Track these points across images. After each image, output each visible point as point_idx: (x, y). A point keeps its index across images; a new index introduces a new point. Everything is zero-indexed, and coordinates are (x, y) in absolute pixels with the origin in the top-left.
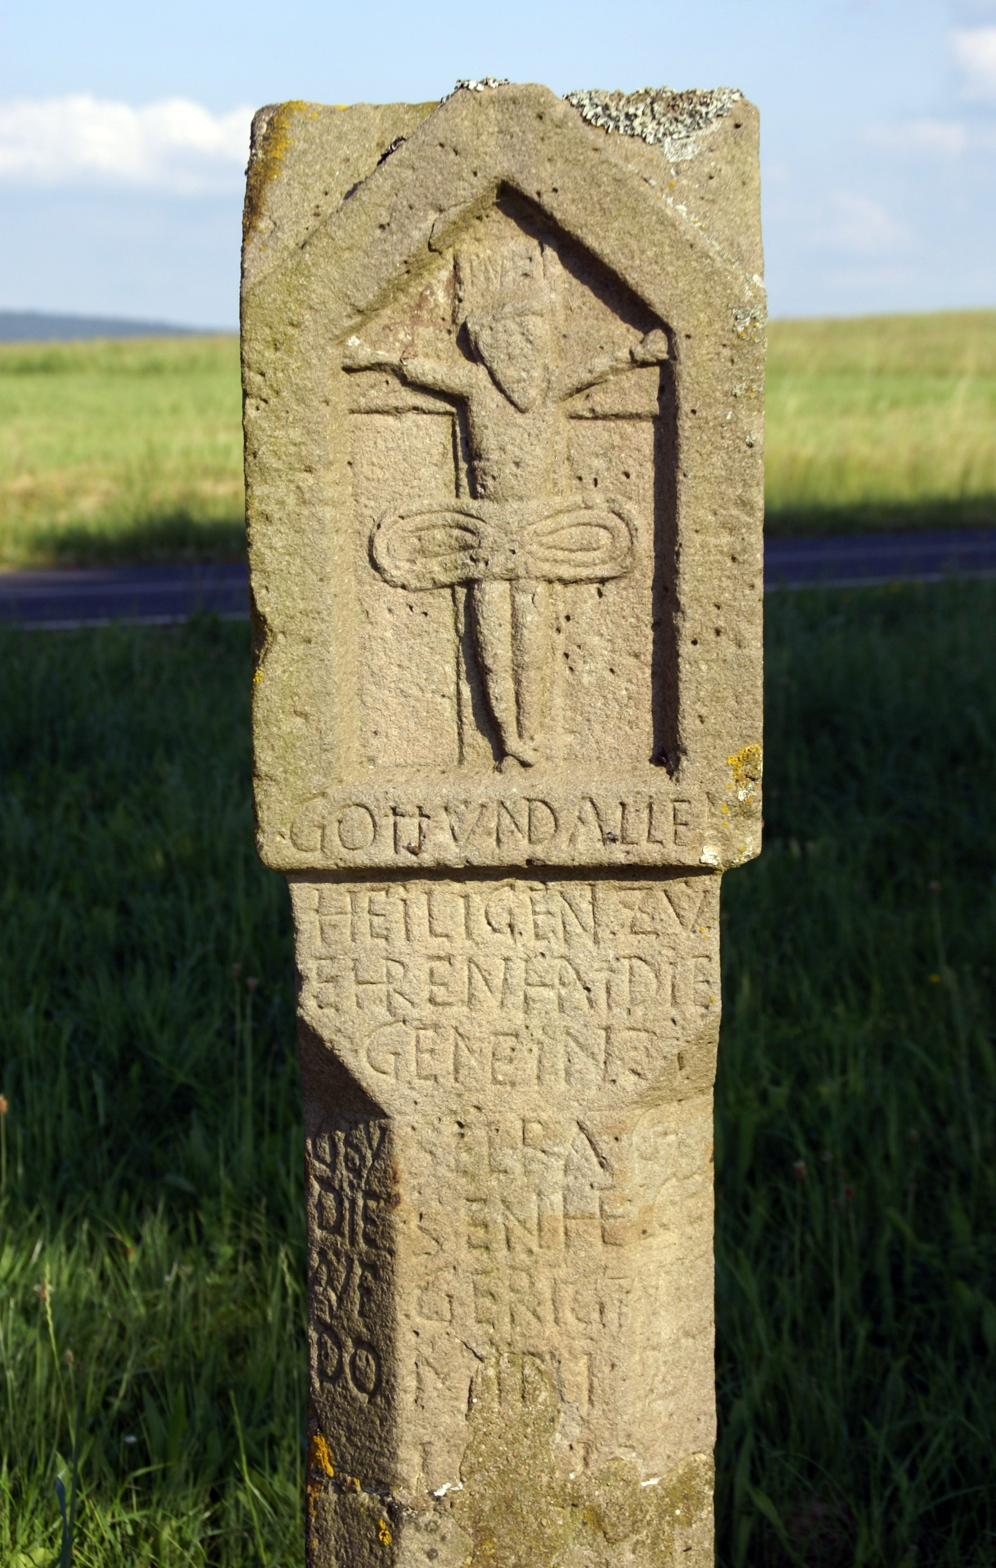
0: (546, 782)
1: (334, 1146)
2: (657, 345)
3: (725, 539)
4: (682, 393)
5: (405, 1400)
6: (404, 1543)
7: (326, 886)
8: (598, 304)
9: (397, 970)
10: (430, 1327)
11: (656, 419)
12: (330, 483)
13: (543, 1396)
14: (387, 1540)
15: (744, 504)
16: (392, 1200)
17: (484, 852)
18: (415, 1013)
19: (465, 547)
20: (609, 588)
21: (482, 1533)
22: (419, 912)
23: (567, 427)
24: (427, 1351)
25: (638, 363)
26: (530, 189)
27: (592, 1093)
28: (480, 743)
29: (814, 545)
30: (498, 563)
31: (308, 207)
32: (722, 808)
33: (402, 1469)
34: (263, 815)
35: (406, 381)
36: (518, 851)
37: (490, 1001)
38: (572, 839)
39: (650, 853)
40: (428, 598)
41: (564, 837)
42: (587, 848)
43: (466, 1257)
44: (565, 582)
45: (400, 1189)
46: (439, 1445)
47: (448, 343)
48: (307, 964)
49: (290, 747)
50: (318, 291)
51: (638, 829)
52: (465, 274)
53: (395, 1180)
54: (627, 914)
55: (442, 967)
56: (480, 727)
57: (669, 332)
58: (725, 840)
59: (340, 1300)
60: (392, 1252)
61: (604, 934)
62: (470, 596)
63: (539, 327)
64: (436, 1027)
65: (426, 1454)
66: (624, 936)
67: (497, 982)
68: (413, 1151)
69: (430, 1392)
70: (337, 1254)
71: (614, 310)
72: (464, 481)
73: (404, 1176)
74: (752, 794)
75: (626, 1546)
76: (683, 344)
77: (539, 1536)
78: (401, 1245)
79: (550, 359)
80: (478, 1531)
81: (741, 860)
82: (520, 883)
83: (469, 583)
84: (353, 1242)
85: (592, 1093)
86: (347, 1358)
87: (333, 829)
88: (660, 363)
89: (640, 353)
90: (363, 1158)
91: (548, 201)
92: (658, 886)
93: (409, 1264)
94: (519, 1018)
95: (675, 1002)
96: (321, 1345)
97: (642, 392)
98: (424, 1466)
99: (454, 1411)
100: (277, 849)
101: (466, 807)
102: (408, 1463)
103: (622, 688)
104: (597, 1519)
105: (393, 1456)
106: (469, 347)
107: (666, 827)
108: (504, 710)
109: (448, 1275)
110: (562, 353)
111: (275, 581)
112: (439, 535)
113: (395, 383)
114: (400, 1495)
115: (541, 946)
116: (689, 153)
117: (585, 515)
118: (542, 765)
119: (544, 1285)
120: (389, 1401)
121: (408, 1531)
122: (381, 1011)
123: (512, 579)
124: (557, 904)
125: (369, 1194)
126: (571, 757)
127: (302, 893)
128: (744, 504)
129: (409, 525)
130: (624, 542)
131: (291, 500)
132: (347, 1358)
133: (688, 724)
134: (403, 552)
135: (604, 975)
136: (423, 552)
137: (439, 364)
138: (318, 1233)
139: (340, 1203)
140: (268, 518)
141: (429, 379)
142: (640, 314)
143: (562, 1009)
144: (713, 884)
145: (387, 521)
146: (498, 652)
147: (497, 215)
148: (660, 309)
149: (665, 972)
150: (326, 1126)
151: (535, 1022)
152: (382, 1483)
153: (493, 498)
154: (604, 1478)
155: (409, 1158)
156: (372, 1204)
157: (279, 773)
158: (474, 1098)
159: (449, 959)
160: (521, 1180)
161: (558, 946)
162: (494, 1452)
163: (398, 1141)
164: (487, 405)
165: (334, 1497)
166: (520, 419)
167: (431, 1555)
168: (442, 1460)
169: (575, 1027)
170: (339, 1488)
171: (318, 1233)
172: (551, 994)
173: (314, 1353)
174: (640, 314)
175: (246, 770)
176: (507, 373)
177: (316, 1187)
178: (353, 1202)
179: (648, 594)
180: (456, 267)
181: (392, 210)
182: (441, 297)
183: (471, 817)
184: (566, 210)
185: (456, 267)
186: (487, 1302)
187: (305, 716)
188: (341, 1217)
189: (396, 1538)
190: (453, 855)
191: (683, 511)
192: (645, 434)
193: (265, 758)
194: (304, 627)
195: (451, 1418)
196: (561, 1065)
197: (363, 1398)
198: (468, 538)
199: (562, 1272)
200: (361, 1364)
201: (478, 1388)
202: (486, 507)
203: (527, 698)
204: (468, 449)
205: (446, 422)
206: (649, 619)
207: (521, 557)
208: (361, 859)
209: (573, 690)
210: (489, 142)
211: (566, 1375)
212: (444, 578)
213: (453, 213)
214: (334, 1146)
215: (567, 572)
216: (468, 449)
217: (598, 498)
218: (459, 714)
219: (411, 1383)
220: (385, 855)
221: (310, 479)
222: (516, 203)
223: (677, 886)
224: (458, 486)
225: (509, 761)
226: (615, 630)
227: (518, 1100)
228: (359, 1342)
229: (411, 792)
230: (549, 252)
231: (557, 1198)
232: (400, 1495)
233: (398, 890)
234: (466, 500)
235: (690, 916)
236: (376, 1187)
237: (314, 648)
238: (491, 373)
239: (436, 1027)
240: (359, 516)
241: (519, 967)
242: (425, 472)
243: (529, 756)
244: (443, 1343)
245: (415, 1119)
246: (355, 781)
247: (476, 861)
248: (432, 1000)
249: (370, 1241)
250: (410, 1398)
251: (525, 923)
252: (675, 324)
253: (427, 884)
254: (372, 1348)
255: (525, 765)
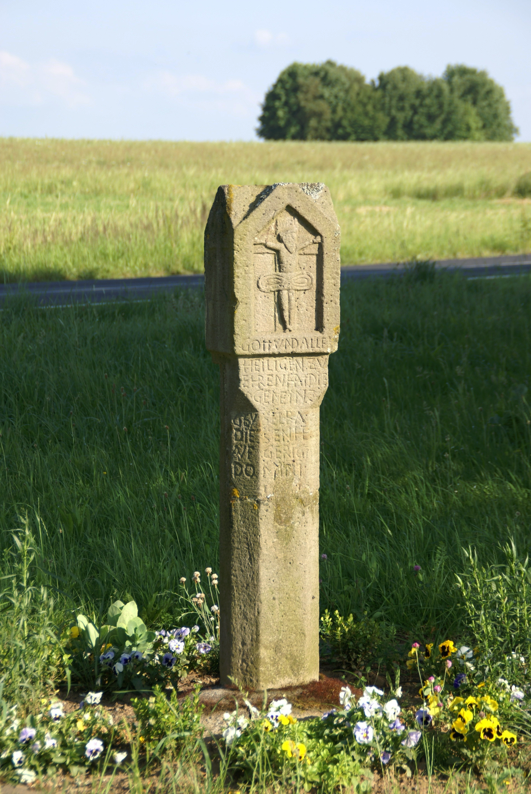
0: (296, 334)
1: (240, 421)
2: (319, 239)
3: (333, 281)
4: (324, 249)
5: (261, 476)
6: (261, 508)
7: (246, 359)
8: (305, 230)
9: (261, 378)
10: (267, 459)
11: (317, 255)
12: (251, 269)
13: (291, 474)
14: (257, 508)
15: (337, 273)
16: (258, 431)
17: (283, 350)
18: (264, 388)
19: (278, 283)
20: (306, 292)
21: (278, 505)
22: (266, 364)
23: (298, 256)
24: (266, 464)
25: (314, 243)
26: (294, 206)
27: (301, 405)
28: (280, 326)
29: (355, 281)
30: (286, 286)
31: (242, 209)
32: (332, 340)
33: (260, 492)
34: (236, 343)
35: (266, 247)
36: (290, 350)
37: (280, 384)
38: (301, 347)
39: (317, 350)
40: (269, 294)
41: (299, 346)
42: (304, 349)
43: (275, 443)
44: (298, 290)
45: (261, 428)
46: (268, 486)
47: (275, 239)
48: (242, 377)
49: (242, 327)
50: (250, 228)
51: (315, 345)
52: (278, 224)
53: (260, 426)
54: (309, 364)
55: (270, 377)
56: (280, 323)
57: (321, 236)
58: (332, 347)
59: (242, 456)
60: (258, 443)
61: (305, 369)
62: (279, 294)
63: (295, 235)
64: (269, 391)
65: (265, 488)
66: (309, 369)
67: (282, 380)
68: (263, 419)
69: (267, 474)
70: (241, 446)
71: (309, 231)
72: (278, 269)
73: (262, 425)
74: (337, 336)
75: (307, 507)
76: (325, 239)
77: (290, 505)
78: (261, 441)
79: (296, 242)
80: (277, 505)
81: (334, 351)
82: (288, 358)
83: (279, 291)
84: (246, 442)
85: (301, 405)
86: (244, 469)
87: (251, 346)
88: (319, 243)
89: (315, 241)
90: (250, 422)
91: (298, 209)
92: (316, 358)
93: (262, 445)
94: (286, 388)
95: (319, 384)
96: (235, 467)
97: (315, 249)
98: (265, 491)
99: (272, 478)
100: (239, 350)
101: (279, 340)
102: (262, 490)
103: (309, 314)
104: (302, 502)
105: (258, 489)
106: (280, 239)
107: (320, 344)
108: (287, 319)
109: (271, 447)
110: (298, 241)
111: (240, 291)
112: (272, 280)
113: (264, 247)
114: (260, 498)
115: (291, 372)
116: (317, 197)
117: (302, 276)
118: (293, 331)
119: (291, 449)
120: (257, 477)
121: (262, 506)
122: (257, 387)
123: (288, 290)
124: (295, 362)
125: (252, 430)
126: (298, 329)
127: (241, 361)
128: (337, 273)
129: (266, 278)
130: (310, 282)
131: (243, 273)
132: (244, 469)
133: (325, 321)
134: (264, 284)
135: (304, 378)
136: (268, 284)
137: (273, 243)
138: (235, 442)
139: (242, 433)
140: (238, 277)
141: (272, 246)
142: (314, 231)
143: (295, 386)
144: (327, 357)
145: (262, 277)
146: (286, 306)
147: (285, 211)
148: (320, 232)
149: (316, 378)
150: (239, 415)
151: (290, 389)
152: (255, 496)
153: (285, 272)
154: (303, 492)
155: (262, 420)
156: (252, 432)
157: (240, 333)
158: (277, 407)
159: (272, 375)
160: (286, 425)
161: (295, 372)
162: (280, 487)
163: (260, 417)
164: (284, 253)
165: (239, 502)
166: (291, 255)
167: (267, 511)
168: (269, 489)
169: (298, 390)
170: (241, 499)
171: (235, 442)
172: (293, 383)
173: (233, 470)
174: (314, 231)
175: (232, 332)
176: (288, 245)
177: (234, 431)
178: (246, 433)
179: (315, 293)
180: (276, 222)
181: (266, 211)
182: (273, 229)
183: (280, 342)
184: (301, 211)
185: (276, 222)
186: (279, 453)
187: (245, 321)
188: (242, 437)
189: (259, 507)
190: (276, 351)
191: (324, 275)
192: (314, 258)
193: (237, 330)
194: (245, 301)
195: (271, 480)
196: (295, 398)
197: (249, 478)
198: (279, 281)
199: (295, 446)
200: (249, 470)
201: (277, 472)
202: (284, 274)
203: (292, 316)
204: (279, 261)
205: (273, 256)
206: (315, 299)
207: (291, 285)
208: (257, 352)
209: (299, 314)
210: (286, 196)
211: (296, 469)
212: (273, 290)
213: (278, 211)
214: (240, 421)
215: (298, 288)
216: (279, 261)
217: (305, 272)
218: (275, 320)
219: (263, 472)
220: (262, 351)
221: (247, 268)
222: (290, 209)
223: (320, 358)
224: (276, 270)
225: (287, 330)
226: (308, 301)
227: (286, 407)
228: (248, 465)
229: (268, 337)
230: (296, 219)
231: (294, 429)
232: (260, 498)
233: (261, 359)
234: (278, 272)
235: (322, 364)
236: (254, 428)
237: (248, 305)
238: (285, 245)
239: (269, 391)
240: (255, 276)
241: (287, 376)
242: (269, 267)
243: (291, 329)
244: (269, 463)
245: (264, 412)
246: (254, 335)
247: (281, 352)
248: (268, 385)
249: (251, 440)
250: (262, 475)
251: (288, 367)
252: (323, 235)
253: (268, 358)
254: (252, 465)
255: (290, 331)
